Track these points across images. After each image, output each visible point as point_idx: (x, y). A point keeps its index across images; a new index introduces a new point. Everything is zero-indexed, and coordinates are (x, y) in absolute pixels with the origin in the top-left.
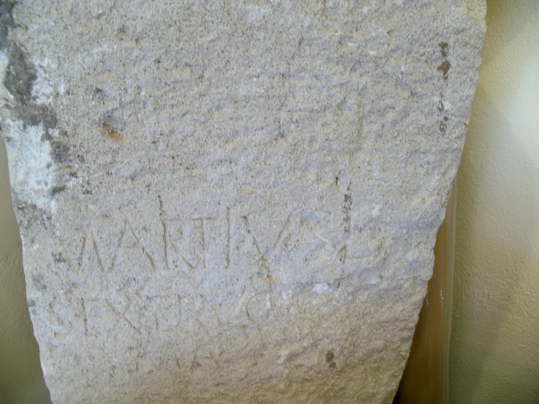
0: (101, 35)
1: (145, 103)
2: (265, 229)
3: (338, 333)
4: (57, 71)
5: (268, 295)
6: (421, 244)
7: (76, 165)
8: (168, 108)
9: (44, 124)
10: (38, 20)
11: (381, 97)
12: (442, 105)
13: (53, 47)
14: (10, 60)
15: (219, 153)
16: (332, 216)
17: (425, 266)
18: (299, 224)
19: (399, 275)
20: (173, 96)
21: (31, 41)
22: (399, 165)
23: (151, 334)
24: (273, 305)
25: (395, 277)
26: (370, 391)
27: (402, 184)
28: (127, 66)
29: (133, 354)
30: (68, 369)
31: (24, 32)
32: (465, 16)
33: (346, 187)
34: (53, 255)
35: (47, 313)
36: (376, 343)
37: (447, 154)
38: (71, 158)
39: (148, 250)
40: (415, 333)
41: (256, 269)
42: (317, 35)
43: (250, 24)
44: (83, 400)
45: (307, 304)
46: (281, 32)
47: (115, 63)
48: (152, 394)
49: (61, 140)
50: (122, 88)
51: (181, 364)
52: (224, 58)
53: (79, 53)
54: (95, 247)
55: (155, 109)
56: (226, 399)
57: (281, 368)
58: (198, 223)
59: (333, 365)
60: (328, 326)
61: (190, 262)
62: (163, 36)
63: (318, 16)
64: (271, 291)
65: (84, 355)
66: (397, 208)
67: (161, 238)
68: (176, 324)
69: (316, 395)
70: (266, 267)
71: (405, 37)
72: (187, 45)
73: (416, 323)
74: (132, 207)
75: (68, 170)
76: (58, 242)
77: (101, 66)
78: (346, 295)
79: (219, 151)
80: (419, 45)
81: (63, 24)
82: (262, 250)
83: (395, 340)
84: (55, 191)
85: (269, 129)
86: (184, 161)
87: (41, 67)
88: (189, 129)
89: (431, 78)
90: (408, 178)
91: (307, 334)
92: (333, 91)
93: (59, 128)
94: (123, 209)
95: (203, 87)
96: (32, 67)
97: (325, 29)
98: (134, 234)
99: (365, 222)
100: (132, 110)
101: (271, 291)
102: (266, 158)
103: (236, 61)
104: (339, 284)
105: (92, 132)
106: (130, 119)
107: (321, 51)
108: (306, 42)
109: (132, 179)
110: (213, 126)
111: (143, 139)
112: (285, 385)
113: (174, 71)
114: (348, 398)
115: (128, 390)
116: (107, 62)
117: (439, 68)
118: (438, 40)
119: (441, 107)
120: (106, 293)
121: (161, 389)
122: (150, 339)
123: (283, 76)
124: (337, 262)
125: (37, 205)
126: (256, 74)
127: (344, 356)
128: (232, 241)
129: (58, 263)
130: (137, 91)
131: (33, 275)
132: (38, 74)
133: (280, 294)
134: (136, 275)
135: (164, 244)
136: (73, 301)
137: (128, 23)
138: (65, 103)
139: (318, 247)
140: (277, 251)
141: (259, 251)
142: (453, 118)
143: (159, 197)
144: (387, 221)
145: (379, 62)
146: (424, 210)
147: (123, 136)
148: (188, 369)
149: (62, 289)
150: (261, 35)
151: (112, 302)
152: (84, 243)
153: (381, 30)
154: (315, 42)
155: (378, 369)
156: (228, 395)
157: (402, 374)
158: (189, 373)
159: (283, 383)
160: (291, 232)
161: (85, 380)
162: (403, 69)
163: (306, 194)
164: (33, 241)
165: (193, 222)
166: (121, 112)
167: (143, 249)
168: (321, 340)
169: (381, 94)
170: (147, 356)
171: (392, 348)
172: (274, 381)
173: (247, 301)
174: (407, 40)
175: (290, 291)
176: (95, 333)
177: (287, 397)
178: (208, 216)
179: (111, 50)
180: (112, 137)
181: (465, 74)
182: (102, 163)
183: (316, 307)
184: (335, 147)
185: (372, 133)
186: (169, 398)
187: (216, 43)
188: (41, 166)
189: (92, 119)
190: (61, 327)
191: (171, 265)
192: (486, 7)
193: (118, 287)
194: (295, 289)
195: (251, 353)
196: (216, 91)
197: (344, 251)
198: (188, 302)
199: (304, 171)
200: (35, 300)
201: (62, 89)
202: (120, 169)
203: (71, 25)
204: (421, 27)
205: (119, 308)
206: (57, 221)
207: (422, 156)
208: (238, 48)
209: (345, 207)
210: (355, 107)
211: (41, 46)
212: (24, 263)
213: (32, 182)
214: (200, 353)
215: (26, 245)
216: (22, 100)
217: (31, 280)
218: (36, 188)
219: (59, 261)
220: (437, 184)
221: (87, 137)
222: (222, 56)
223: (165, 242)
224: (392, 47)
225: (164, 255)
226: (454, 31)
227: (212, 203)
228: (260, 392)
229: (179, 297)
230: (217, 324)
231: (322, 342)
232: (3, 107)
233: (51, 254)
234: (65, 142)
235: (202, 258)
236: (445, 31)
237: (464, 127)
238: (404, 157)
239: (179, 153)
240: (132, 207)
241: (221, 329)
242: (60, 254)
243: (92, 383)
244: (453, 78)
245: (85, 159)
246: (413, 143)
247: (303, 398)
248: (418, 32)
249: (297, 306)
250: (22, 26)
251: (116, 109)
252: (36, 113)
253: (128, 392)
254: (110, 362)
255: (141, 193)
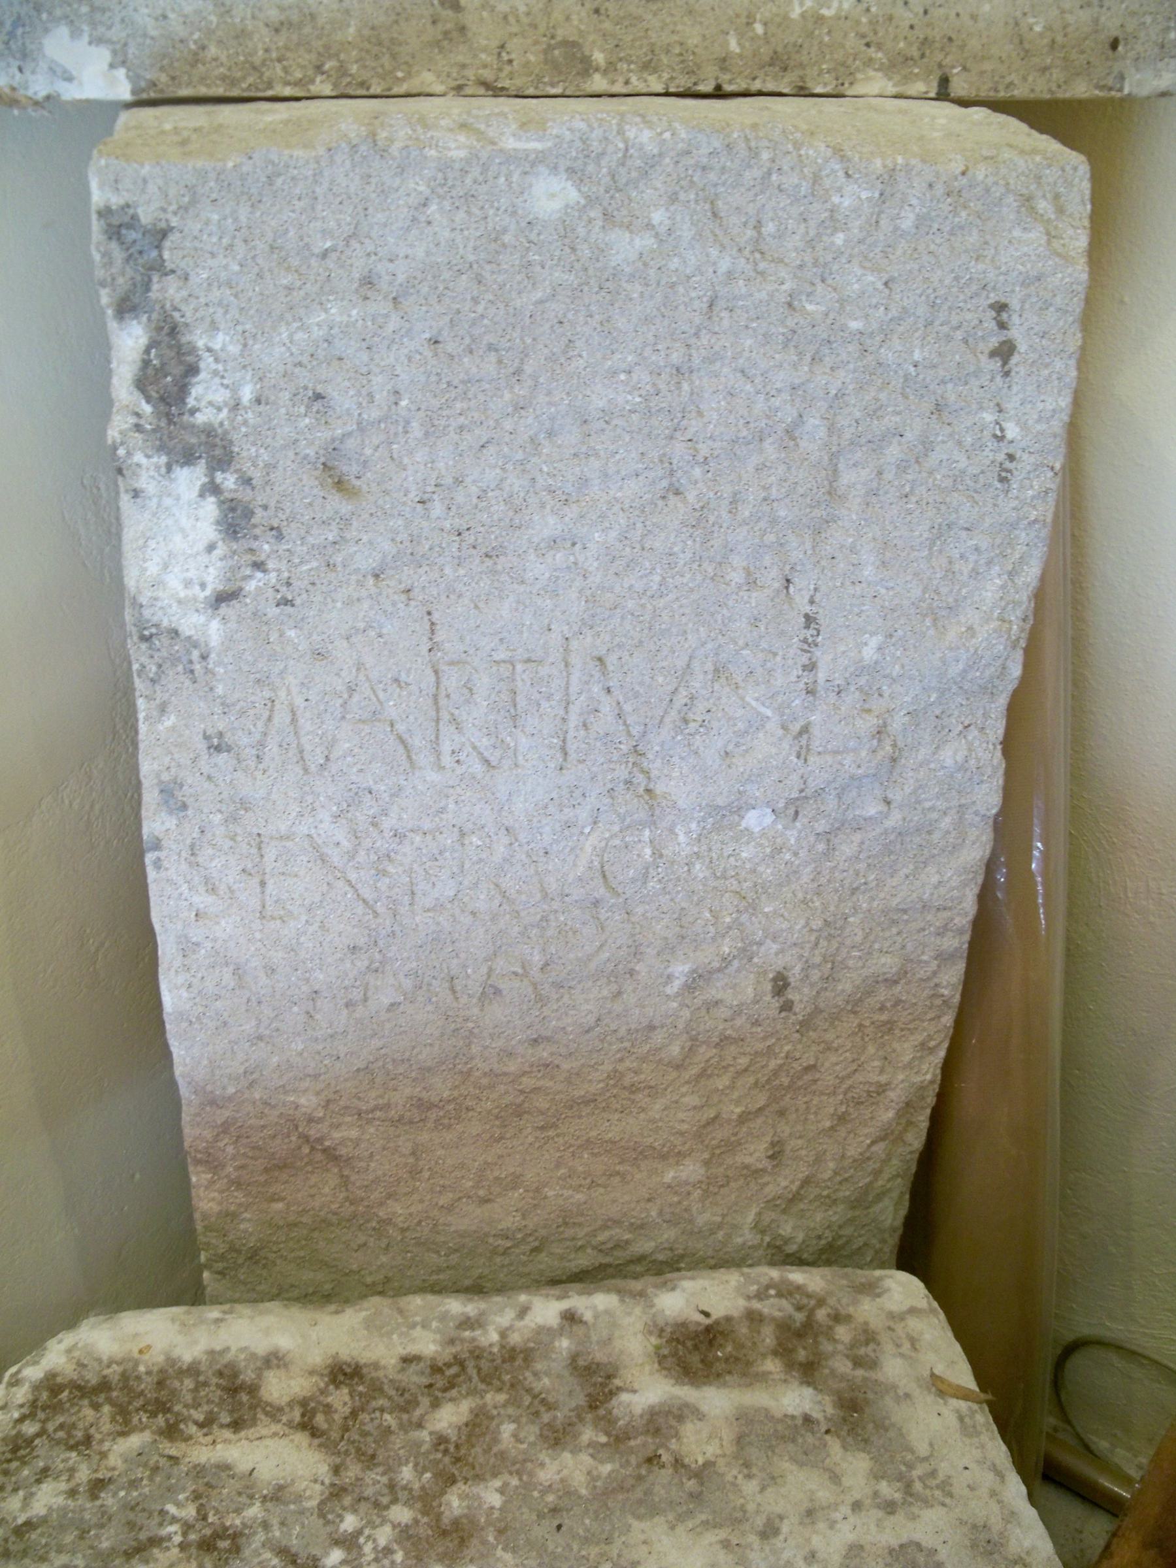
0: (327, 289)
1: (408, 422)
2: (641, 683)
3: (798, 927)
4: (240, 360)
5: (647, 832)
6: (972, 727)
7: (266, 547)
8: (452, 433)
9: (207, 463)
10: (210, 262)
11: (875, 412)
12: (1002, 430)
13: (234, 312)
14: (151, 338)
15: (548, 524)
16: (778, 659)
17: (982, 782)
18: (710, 677)
19: (926, 800)
20: (462, 410)
21: (193, 303)
22: (916, 553)
23: (398, 917)
24: (658, 854)
25: (919, 802)
26: (874, 1078)
27: (924, 592)
28: (374, 349)
29: (359, 964)
30: (218, 997)
31: (181, 284)
32: (1041, 249)
33: (807, 598)
34: (206, 737)
35: (184, 866)
36: (883, 960)
37: (1017, 532)
38: (257, 531)
39: (401, 727)
40: (972, 944)
41: (622, 772)
42: (744, 290)
43: (614, 268)
44: (245, 1072)
45: (729, 856)
46: (673, 286)
47: (352, 343)
48: (394, 1061)
49: (239, 495)
50: (364, 392)
51: (458, 988)
52: (563, 334)
53: (283, 323)
54: (294, 720)
55: (427, 434)
56: (552, 1078)
57: (675, 1005)
58: (505, 670)
59: (787, 1007)
60: (775, 912)
61: (486, 754)
62: (446, 292)
63: (746, 252)
64: (653, 823)
65: (253, 965)
66: (915, 647)
67: (430, 701)
68: (452, 893)
69: (752, 1080)
70: (642, 771)
71: (918, 292)
72: (492, 310)
73: (970, 917)
74: (372, 634)
75: (249, 558)
76: (218, 710)
77: (325, 350)
78: (812, 839)
79: (552, 520)
80: (950, 308)
81: (256, 270)
82: (636, 731)
83: (925, 958)
84: (223, 598)
85: (652, 475)
86: (480, 540)
87: (209, 350)
88: (492, 475)
89: (977, 374)
90: (935, 582)
91: (730, 928)
92: (776, 402)
93: (236, 471)
94: (353, 640)
95: (521, 391)
96: (193, 350)
97: (759, 279)
98: (374, 692)
99: (847, 675)
100: (383, 437)
101: (653, 823)
102: (643, 536)
103: (587, 341)
104: (797, 813)
105: (301, 480)
106: (377, 454)
107: (752, 320)
108: (722, 304)
109: (377, 576)
110: (541, 470)
111: (402, 494)
112: (683, 1048)
113: (466, 360)
114: (822, 1094)
115: (343, 1050)
116: (336, 340)
117: (993, 354)
118: (988, 297)
119: (999, 433)
120: (311, 820)
121: (414, 1048)
122: (396, 928)
123: (678, 370)
124: (791, 761)
125: (180, 629)
126: (624, 366)
127: (812, 985)
128: (575, 709)
129: (215, 754)
130: (392, 399)
131: (161, 782)
132: (202, 365)
133: (671, 830)
134: (376, 783)
135: (434, 713)
136: (239, 839)
137: (379, 267)
138: (251, 421)
139: (751, 726)
140: (666, 733)
141: (629, 734)
142: (1025, 456)
143: (429, 613)
144: (894, 674)
145: (869, 342)
146: (972, 650)
147: (360, 490)
148: (475, 1001)
149: (220, 811)
150: (636, 289)
151: (320, 842)
152: (272, 711)
153: (871, 278)
154: (741, 303)
155: (888, 1027)
156: (558, 1066)
157: (946, 1045)
158: (476, 1011)
159: (678, 1043)
160: (694, 691)
161: (254, 1023)
162: (917, 356)
163: (725, 611)
164: (163, 709)
165: (495, 668)
166: (359, 441)
167: (392, 725)
168: (760, 944)
169: (874, 407)
170: (388, 968)
171: (918, 976)
172: (658, 1038)
173: (603, 844)
174: (923, 298)
175: (693, 826)
176: (282, 913)
177: (687, 1077)
178: (526, 656)
179: (345, 318)
180: (340, 490)
181: (1047, 366)
182: (317, 542)
183: (748, 866)
184: (782, 513)
185: (859, 486)
186: (429, 1069)
187: (547, 305)
188: (195, 549)
189: (302, 455)
190: (210, 899)
191: (447, 760)
192: (1088, 231)
193: (335, 808)
194: (704, 820)
195: (610, 966)
196: (547, 399)
197: (805, 736)
198: (480, 843)
199: (720, 564)
200: (161, 836)
201: (247, 394)
202: (352, 556)
203: (270, 270)
204: (952, 271)
205: (336, 857)
206: (219, 663)
207: (964, 534)
208: (591, 316)
209: (805, 641)
210: (822, 433)
211: (211, 310)
212: (141, 756)
213: (174, 582)
214: (500, 964)
215: (146, 718)
216: (169, 417)
217: (156, 792)
218: (182, 595)
219: (218, 749)
220: (997, 596)
221: (291, 489)
222: (559, 330)
223: (438, 711)
224: (894, 312)
225: (433, 738)
226: (1021, 278)
227: (535, 627)
228: (627, 1064)
229: (462, 834)
230: (539, 896)
231: (763, 949)
232: (130, 429)
233: (201, 736)
234: (247, 499)
235: (512, 744)
236: (1001, 278)
237: (1050, 474)
238: (926, 535)
239: (472, 524)
240: (372, 634)
241: (545, 907)
242: (221, 735)
243: (267, 1032)
244: (1022, 373)
245: (285, 533)
246: (943, 507)
247: (722, 1082)
248: (947, 282)
249: (708, 860)
250: (179, 273)
251: (350, 434)
252: (194, 440)
253: (342, 1055)
254: (307, 980)
255: (394, 604)
